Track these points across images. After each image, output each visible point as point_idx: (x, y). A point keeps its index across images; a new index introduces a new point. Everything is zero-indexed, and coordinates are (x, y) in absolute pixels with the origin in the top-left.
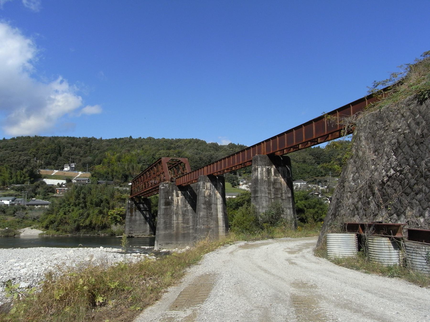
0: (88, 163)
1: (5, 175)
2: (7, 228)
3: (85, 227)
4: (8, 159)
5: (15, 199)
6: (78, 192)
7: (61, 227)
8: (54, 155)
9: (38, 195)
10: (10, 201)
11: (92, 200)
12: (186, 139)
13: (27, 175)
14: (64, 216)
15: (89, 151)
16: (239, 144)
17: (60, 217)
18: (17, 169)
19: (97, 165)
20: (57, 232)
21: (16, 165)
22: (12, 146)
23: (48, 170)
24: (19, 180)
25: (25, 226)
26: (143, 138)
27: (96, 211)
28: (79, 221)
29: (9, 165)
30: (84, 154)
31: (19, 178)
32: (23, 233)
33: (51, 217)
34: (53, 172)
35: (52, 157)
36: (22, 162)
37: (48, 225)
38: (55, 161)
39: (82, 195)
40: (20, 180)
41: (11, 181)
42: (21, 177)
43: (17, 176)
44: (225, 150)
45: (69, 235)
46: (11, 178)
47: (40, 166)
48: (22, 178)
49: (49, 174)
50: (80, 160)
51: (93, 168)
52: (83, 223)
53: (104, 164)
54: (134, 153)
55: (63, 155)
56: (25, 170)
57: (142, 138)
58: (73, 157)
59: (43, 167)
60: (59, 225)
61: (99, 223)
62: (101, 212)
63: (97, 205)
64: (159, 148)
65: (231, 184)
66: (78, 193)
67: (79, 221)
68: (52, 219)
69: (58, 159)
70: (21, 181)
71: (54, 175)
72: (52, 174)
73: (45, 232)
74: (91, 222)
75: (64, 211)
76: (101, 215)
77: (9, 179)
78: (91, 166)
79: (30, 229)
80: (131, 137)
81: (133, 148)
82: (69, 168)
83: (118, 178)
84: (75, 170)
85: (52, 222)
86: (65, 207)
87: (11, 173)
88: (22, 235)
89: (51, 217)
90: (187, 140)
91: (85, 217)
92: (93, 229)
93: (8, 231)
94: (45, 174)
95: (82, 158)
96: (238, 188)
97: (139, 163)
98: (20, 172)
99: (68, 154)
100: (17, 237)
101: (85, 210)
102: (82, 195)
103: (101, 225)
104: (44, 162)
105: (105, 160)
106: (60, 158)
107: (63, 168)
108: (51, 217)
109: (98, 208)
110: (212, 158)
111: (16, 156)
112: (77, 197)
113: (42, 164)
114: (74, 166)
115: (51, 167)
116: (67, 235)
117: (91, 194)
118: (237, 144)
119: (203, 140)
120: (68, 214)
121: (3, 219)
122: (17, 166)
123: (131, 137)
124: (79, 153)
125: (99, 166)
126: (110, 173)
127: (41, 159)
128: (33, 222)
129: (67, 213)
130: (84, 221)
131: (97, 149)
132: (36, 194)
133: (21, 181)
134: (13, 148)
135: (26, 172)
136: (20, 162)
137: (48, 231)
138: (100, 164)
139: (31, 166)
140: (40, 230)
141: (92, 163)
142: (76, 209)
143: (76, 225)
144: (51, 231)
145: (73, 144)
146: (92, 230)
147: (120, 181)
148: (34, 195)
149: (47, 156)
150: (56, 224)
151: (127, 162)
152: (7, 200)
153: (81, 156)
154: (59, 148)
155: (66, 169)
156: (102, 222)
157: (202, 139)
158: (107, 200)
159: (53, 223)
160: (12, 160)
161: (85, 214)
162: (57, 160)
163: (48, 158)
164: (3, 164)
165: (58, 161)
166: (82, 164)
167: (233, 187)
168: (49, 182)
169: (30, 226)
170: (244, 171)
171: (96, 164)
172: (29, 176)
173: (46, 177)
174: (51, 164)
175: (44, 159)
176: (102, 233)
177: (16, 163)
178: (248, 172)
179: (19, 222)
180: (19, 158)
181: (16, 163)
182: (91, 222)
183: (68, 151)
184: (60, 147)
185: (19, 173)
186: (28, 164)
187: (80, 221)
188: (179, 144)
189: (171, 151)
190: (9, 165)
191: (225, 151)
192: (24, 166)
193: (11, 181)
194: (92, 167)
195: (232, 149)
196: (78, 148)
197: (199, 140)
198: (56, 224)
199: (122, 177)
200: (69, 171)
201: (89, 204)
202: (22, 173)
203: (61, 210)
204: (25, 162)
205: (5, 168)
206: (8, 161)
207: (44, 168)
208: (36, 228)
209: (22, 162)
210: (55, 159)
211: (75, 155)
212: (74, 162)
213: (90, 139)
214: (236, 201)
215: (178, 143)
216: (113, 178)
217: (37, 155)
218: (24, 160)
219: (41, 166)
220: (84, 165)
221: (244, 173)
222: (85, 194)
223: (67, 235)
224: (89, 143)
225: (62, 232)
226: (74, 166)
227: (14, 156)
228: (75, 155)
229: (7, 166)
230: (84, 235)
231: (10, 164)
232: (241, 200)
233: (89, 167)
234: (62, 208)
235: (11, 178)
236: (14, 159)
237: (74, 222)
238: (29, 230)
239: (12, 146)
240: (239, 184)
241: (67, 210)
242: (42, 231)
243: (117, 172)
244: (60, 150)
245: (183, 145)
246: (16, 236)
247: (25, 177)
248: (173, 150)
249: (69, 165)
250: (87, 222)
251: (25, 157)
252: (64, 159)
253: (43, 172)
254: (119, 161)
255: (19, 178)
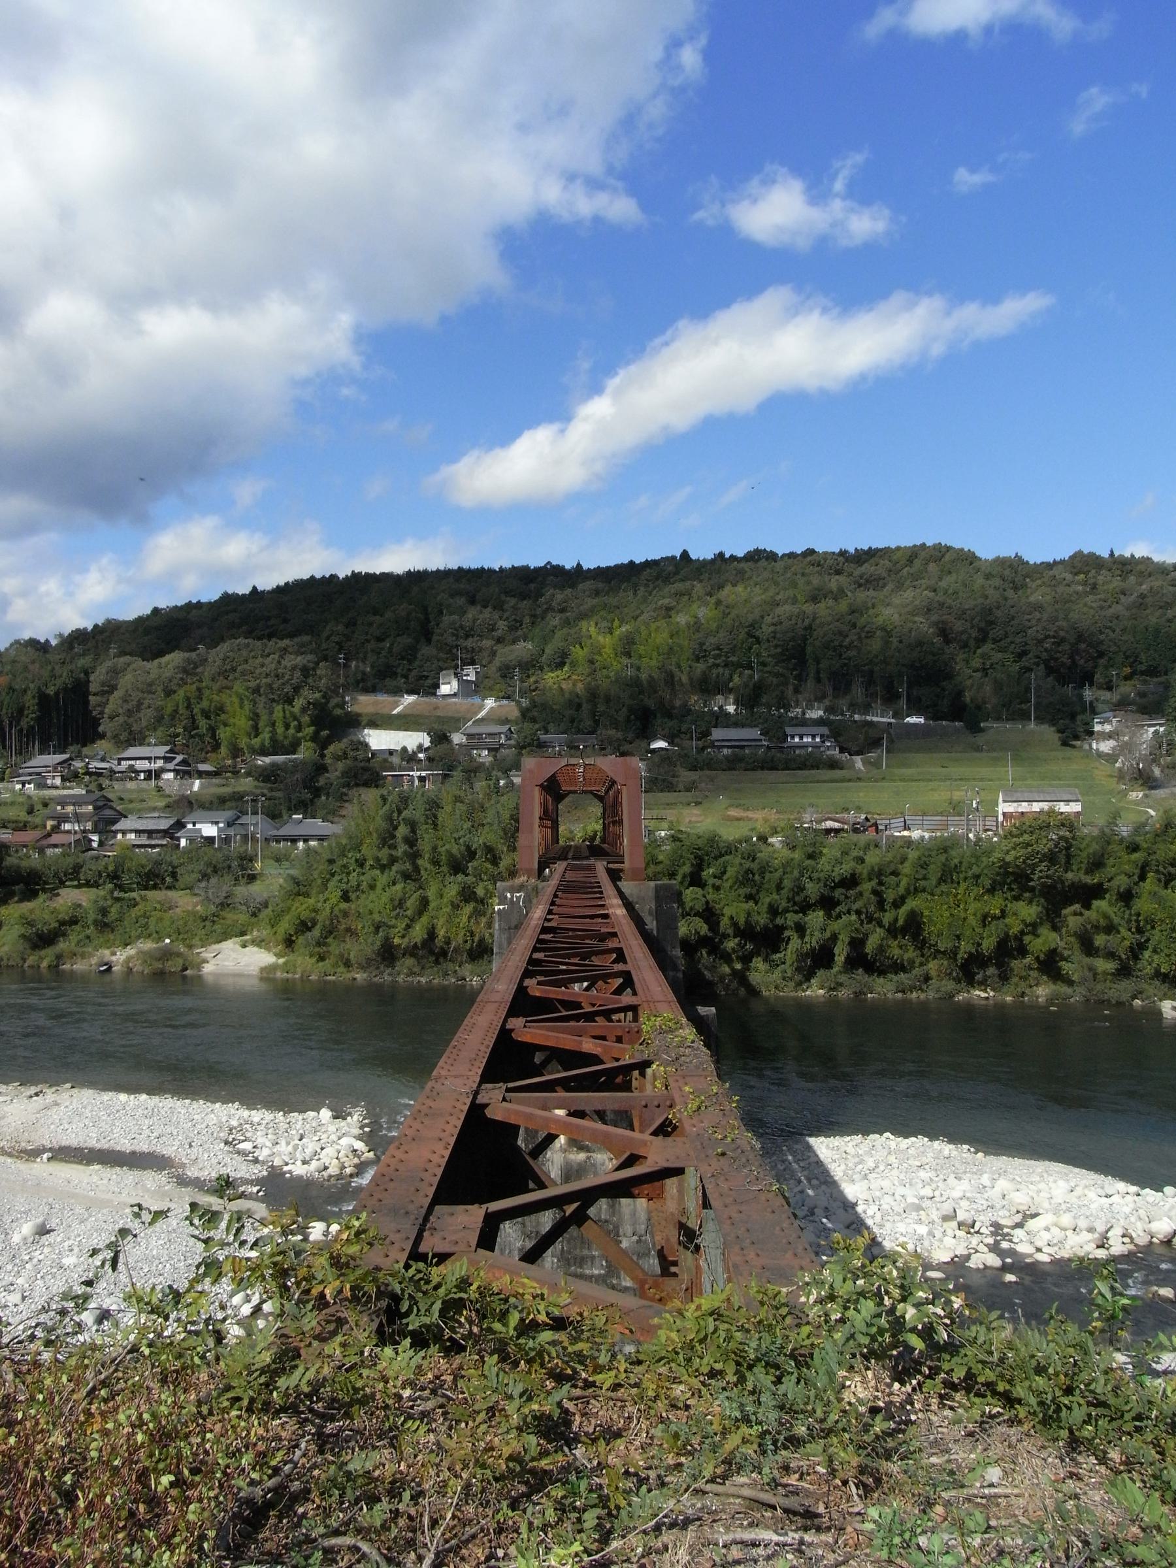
0: (520, 666)
1: (238, 723)
2: (168, 941)
3: (412, 951)
4: (245, 666)
5: (239, 818)
6: (389, 819)
7: (335, 947)
8: (406, 640)
9: (323, 798)
10: (221, 825)
11: (435, 848)
12: (898, 548)
13: (306, 719)
14: (344, 905)
15: (527, 620)
16: (1116, 554)
17: (328, 911)
18: (273, 700)
19: (552, 671)
20: (321, 964)
21: (270, 686)
22: (269, 618)
23: (382, 698)
24: (281, 738)
25: (225, 936)
26: (732, 556)
27: (452, 891)
28: (390, 927)
29: (248, 689)
30: (512, 629)
31: (280, 730)
32: (213, 962)
33: (302, 908)
34: (396, 705)
35: (396, 649)
36: (287, 677)
37: (291, 935)
38: (410, 662)
39: (402, 831)
40: (286, 737)
41: (256, 742)
42: (287, 727)
43: (273, 724)
44: (1055, 582)
45: (360, 976)
46: (256, 731)
47: (358, 682)
48: (291, 731)
49: (385, 711)
50: (493, 654)
51: (536, 682)
52: (403, 937)
53: (573, 665)
54: (682, 619)
55: (435, 638)
56: (299, 703)
57: (727, 556)
58: (469, 643)
59: (369, 684)
60: (326, 938)
61: (460, 940)
62: (467, 895)
63: (457, 867)
64: (778, 598)
65: (1059, 731)
66: (392, 823)
67: (390, 927)
68: (305, 915)
69: (419, 656)
70: (286, 742)
71: (399, 716)
72: (395, 712)
73: (281, 961)
74: (432, 934)
75: (344, 886)
76: (468, 909)
77: (249, 735)
78: (528, 677)
79: (238, 947)
80: (685, 554)
81: (686, 598)
82: (455, 684)
83: (615, 725)
84: (476, 692)
85: (304, 926)
86: (348, 874)
87: (255, 717)
88: (208, 968)
89: (304, 907)
90: (899, 554)
91: (409, 913)
92: (441, 960)
93: (166, 955)
94: (370, 709)
95: (498, 647)
96: (1086, 747)
97: (697, 659)
98: (284, 711)
99: (453, 634)
100: (192, 977)
101: (411, 886)
102: (402, 831)
103: (468, 946)
104: (372, 667)
105: (578, 653)
106: (426, 651)
107: (437, 686)
108: (304, 907)
109: (460, 877)
110: (992, 623)
111: (268, 655)
112: (387, 839)
113: (364, 673)
114: (472, 677)
115: (394, 683)
116: (349, 976)
117: (435, 825)
118: (1105, 554)
119: (962, 550)
120: (358, 897)
121: (158, 907)
122: (272, 689)
123: (685, 554)
124: (493, 629)
125: (559, 672)
126: (584, 705)
127: (361, 655)
128: (254, 920)
129: (353, 896)
130: (408, 926)
131: (556, 607)
132: (317, 792)
133: (286, 742)
134: (270, 623)
135: (304, 710)
136: (283, 677)
137: (292, 957)
138: (561, 665)
139: (317, 688)
140: (268, 949)
141: (534, 666)
142: (383, 879)
143: (379, 943)
144: (300, 960)
145: (474, 596)
146: (437, 962)
147: (620, 735)
148: (309, 796)
149: (381, 645)
150: (316, 932)
151: (655, 654)
152: (212, 823)
153: (499, 640)
154: (422, 616)
155: (445, 689)
156: (472, 934)
157: (958, 541)
158: (489, 849)
159: (309, 929)
160: (258, 671)
161: (412, 903)
162: (415, 658)
163: (384, 653)
164: (230, 684)
165: (417, 663)
166: (500, 669)
167: (1065, 743)
168: (379, 740)
169: (243, 934)
170: (1128, 670)
171: (549, 665)
172: (312, 723)
173: (374, 724)
174: (394, 675)
175: (371, 658)
176: (473, 973)
177: (269, 680)
178: (1142, 673)
179: (204, 919)
180: (279, 662)
181: (269, 680)
182: (432, 934)
183: (454, 623)
184: (425, 609)
185: (281, 714)
186: (310, 680)
187: (394, 927)
188: (867, 568)
189: (822, 605)
190: (248, 689)
191: (1048, 590)
192: (297, 689)
193: (256, 742)
194: (532, 679)
195: (1082, 576)
196: (489, 609)
197: (948, 549)
198: (316, 932)
199: (628, 720)
200: (455, 695)
201: (428, 866)
202: (291, 713)
203: (331, 884)
204: (298, 674)
205: (235, 699)
206: (243, 674)
207: (372, 690)
208: (259, 943)
209: (287, 677)
210: (410, 654)
211: (476, 638)
212: (473, 663)
213: (538, 570)
214: (998, 855)
215: (863, 569)
216: (597, 722)
217: (350, 643)
218: (294, 668)
219: (363, 680)
220: (506, 672)
221: (1126, 678)
222: (413, 825)
223: (349, 976)
224: (532, 586)
225: (336, 965)
226: (472, 677)
227: (262, 656)
228: (476, 638)
229: (241, 691)
230: (409, 979)
231: (252, 684)
232: (1021, 852)
233: (522, 681)
234: (337, 878)
235: (256, 731)
236: (262, 666)
237: (372, 929)
238: (232, 950)
239: (269, 618)
240: (1091, 733)
241: (354, 883)
242: (276, 955)
243: (608, 700)
244: (428, 620)
245: (884, 574)
246: (188, 972)
247: (299, 728)
248: (831, 602)
249: (456, 675)
250: (418, 933)
251: (299, 658)
252: (442, 655)
253: (364, 703)
254: (628, 655)
255: (280, 730)
